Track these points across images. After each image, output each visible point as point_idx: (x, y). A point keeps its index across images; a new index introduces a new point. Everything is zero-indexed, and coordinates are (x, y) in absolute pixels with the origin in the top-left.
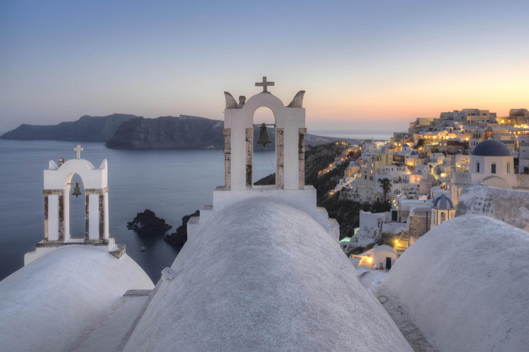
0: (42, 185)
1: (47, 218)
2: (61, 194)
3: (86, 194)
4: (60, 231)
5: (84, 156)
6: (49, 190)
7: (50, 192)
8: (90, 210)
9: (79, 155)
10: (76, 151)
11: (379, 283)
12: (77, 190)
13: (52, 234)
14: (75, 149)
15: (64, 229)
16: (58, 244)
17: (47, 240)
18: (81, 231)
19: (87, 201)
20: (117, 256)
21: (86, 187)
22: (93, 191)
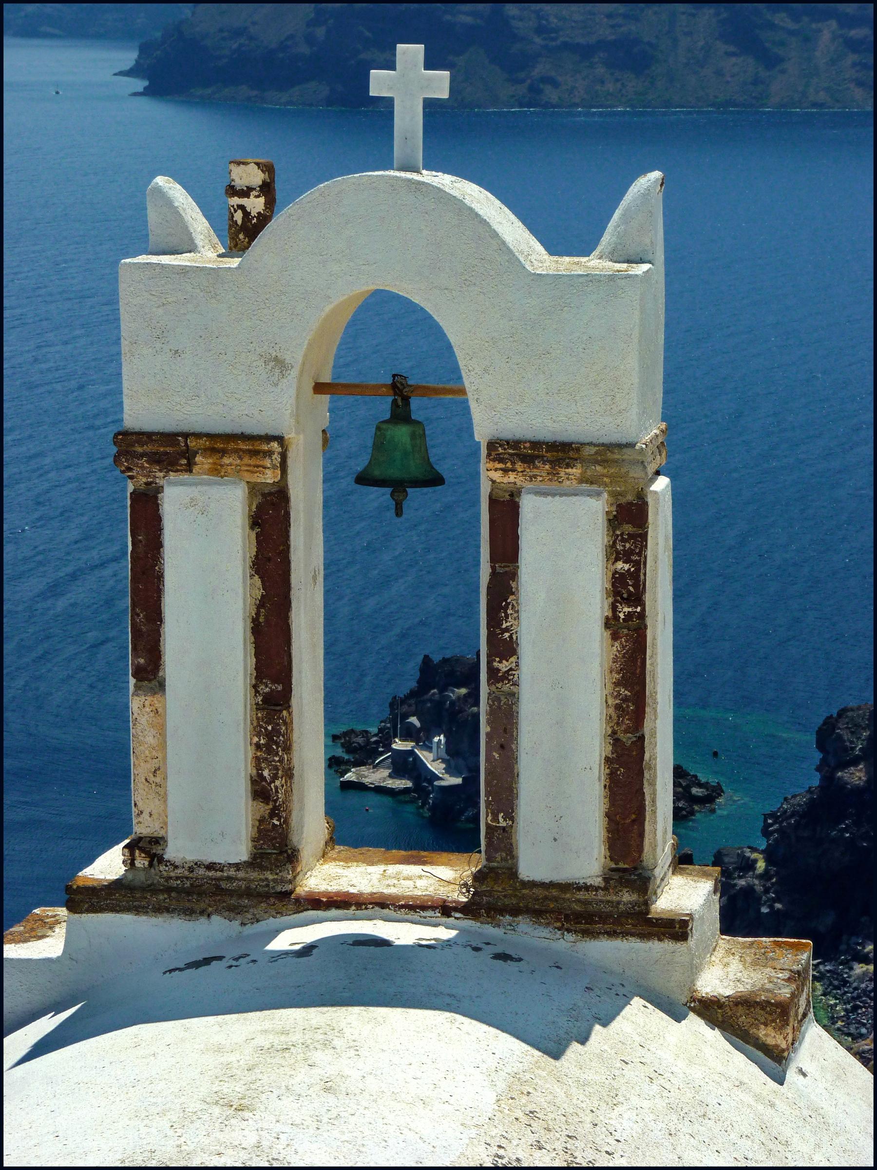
0: (115, 395)
1: (150, 673)
2: (270, 477)
3: (490, 476)
4: (260, 791)
5: (452, 133)
6: (170, 438)
7: (173, 451)
8: (530, 622)
9: (408, 121)
10: (663, 420)
11: (783, 72)
12: (397, 416)
13: (196, 801)
14: (380, 82)
15: (289, 774)
16: (248, 893)
17: (155, 859)
18: (425, 744)
19: (506, 548)
20: (769, 1035)
21: (485, 425)
22: (551, 455)
